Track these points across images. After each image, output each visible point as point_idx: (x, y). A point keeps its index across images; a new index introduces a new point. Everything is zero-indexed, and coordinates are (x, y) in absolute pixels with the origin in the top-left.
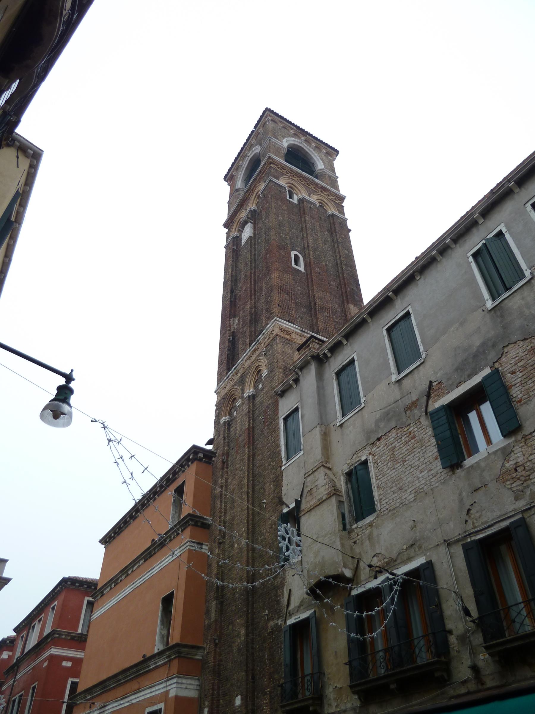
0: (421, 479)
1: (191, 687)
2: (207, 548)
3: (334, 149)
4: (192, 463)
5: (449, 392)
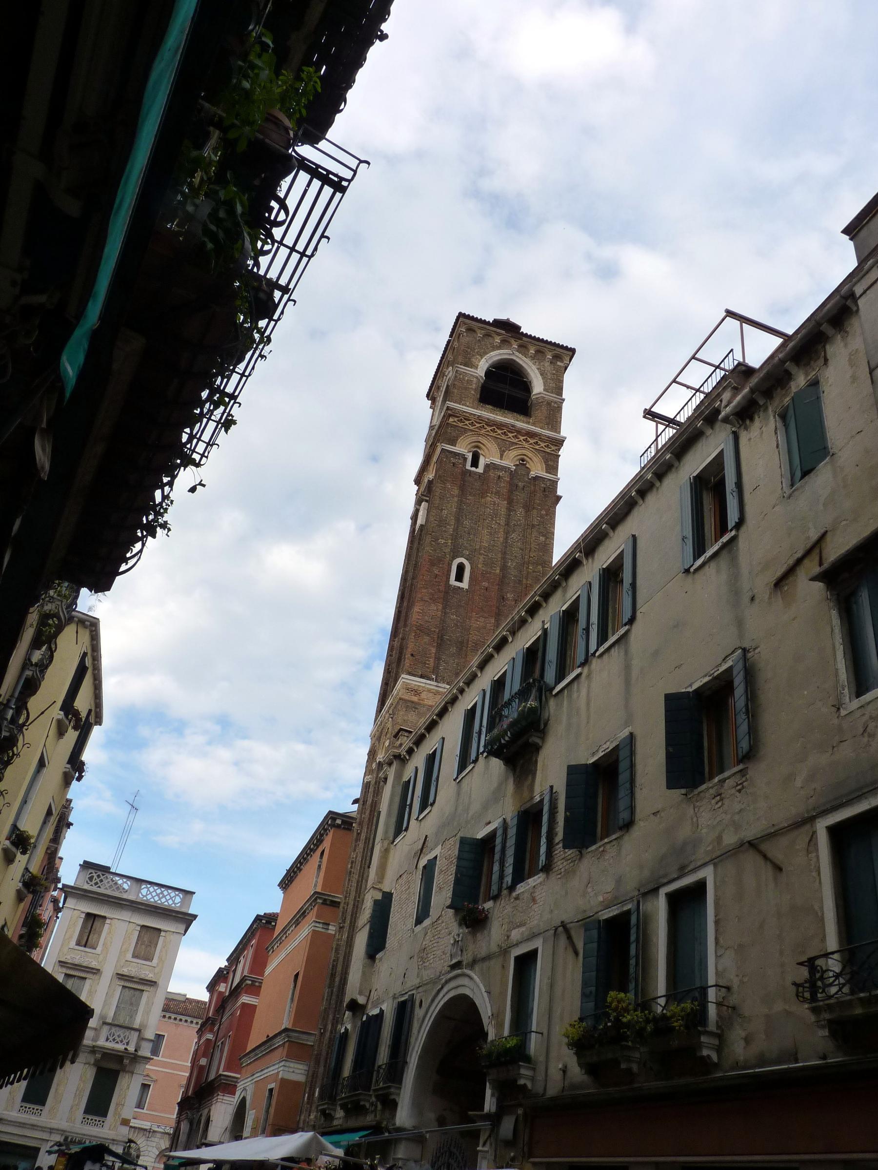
1: (299, 1071)
3: (566, 348)
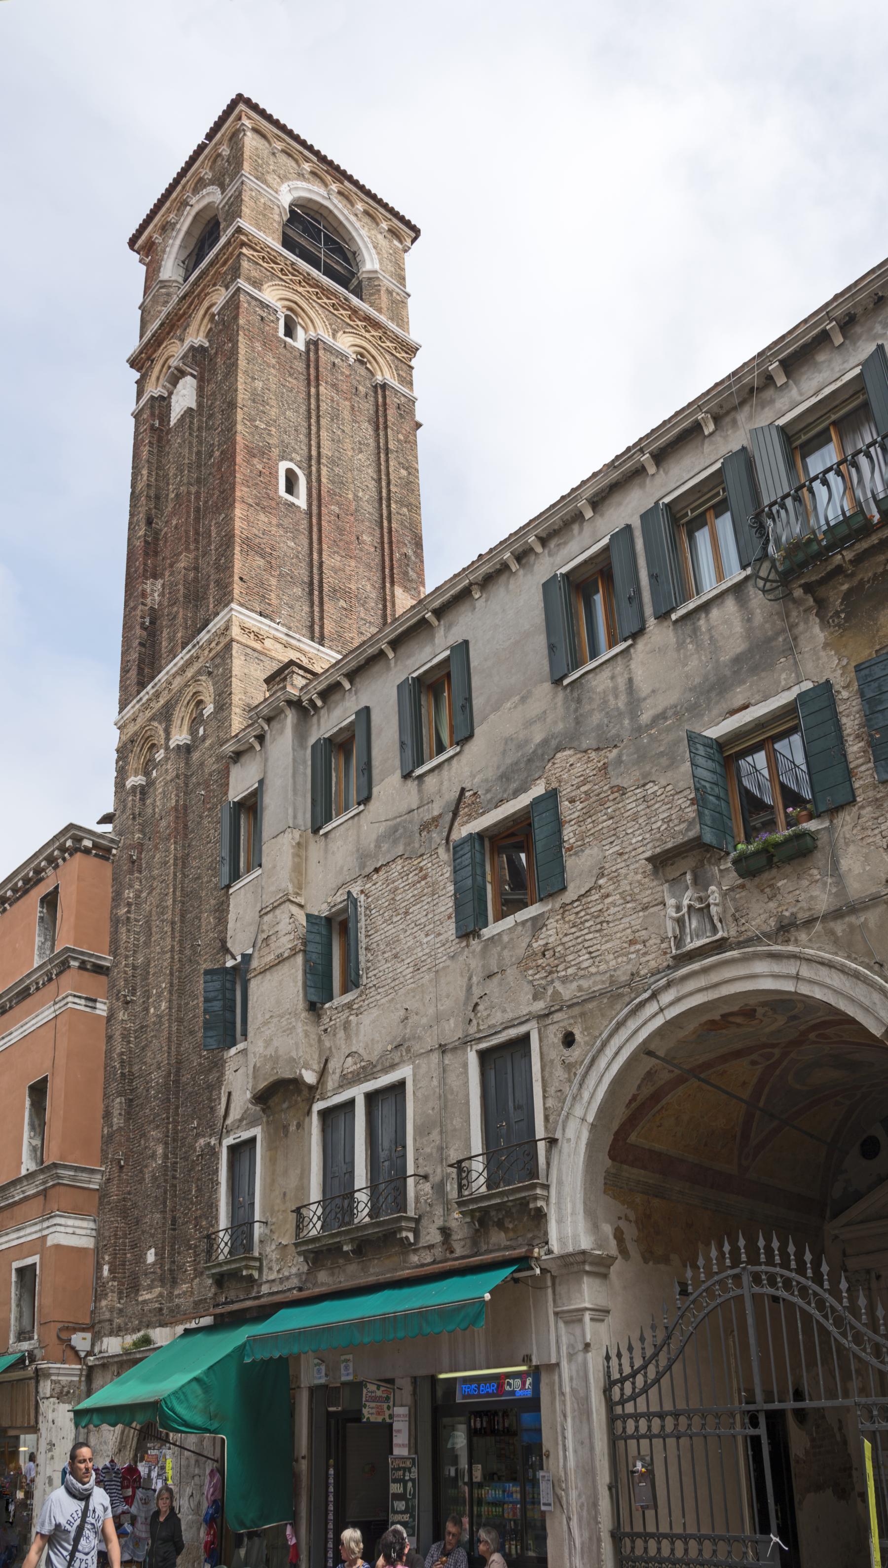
0: (425, 946)
2: (105, 1008)
4: (71, 855)
5: (483, 814)
